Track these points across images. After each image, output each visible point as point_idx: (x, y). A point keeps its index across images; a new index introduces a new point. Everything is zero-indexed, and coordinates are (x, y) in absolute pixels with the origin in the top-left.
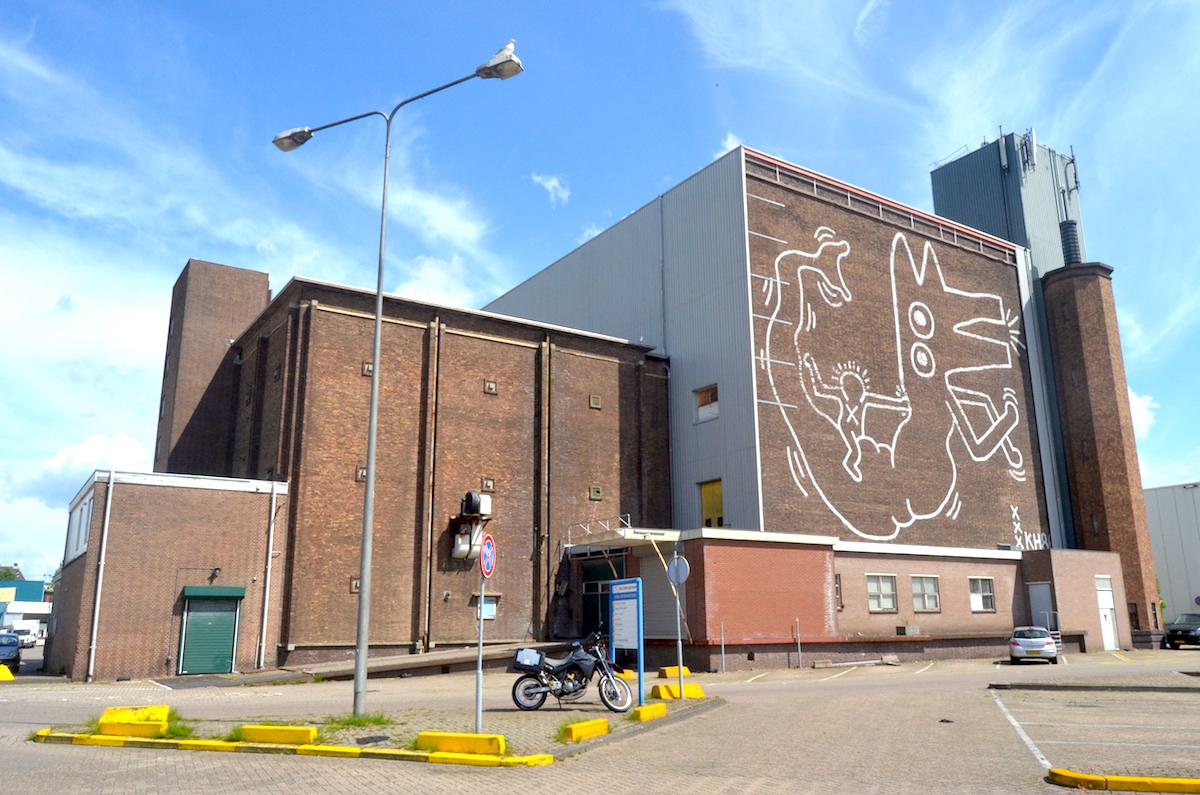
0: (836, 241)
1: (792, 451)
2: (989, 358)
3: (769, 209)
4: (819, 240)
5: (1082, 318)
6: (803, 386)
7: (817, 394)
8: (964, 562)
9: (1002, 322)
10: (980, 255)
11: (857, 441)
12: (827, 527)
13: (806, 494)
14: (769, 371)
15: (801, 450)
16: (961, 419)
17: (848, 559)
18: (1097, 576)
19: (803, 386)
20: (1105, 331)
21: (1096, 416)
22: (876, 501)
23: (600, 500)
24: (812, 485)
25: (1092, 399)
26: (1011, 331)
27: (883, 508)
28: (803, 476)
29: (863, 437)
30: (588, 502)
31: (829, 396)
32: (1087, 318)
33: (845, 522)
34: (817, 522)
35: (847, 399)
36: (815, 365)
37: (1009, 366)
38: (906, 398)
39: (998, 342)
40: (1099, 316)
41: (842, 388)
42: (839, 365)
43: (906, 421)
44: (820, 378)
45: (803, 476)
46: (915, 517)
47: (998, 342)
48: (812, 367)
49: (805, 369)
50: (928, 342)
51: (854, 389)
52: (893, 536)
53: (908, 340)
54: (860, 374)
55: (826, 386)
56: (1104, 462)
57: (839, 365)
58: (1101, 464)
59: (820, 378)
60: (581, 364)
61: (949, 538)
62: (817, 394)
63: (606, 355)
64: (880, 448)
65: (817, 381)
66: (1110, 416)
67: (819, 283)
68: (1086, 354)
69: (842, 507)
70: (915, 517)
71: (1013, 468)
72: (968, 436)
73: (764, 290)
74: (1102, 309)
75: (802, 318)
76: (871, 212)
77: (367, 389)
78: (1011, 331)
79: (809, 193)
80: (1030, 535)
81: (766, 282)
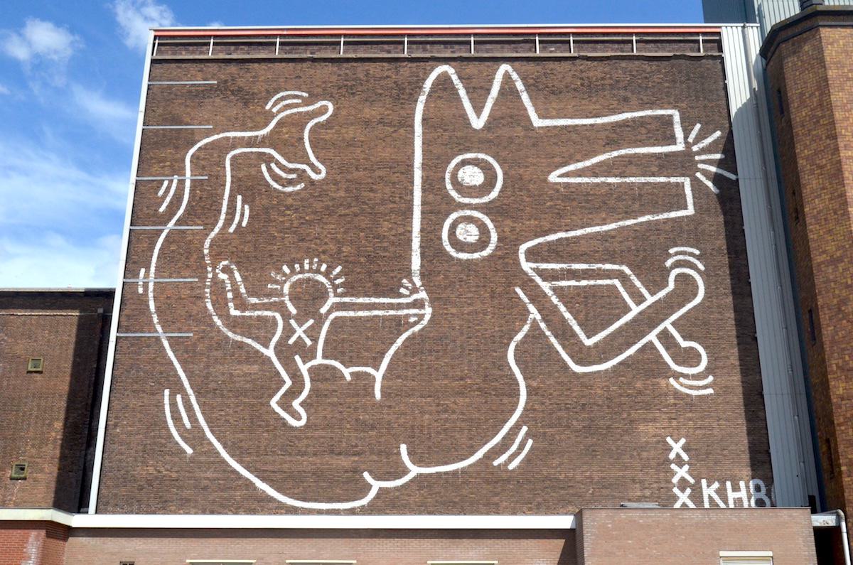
0: (307, 105)
1: (173, 396)
2: (636, 206)
3: (190, 92)
4: (274, 110)
5: (794, 105)
6: (209, 306)
7: (234, 312)
8: (498, 537)
9: (680, 147)
10: (574, 58)
11: (304, 369)
12: (226, 495)
13: (189, 451)
14: (151, 295)
15: (190, 391)
16: (549, 314)
17: (150, 540)
18: (722, 553)
19: (209, 306)
20: (832, 115)
21: (819, 264)
22: (332, 451)
23: (25, 479)
24: (204, 437)
25: (811, 236)
26: (697, 158)
27: (345, 462)
28: (188, 425)
29: (319, 360)
30: (9, 481)
31: (257, 313)
32: (802, 102)
33: (261, 485)
34: (205, 488)
35: (293, 311)
36: (237, 276)
37: (690, 211)
38: (423, 295)
39: (663, 179)
40: (821, 95)
41: (286, 298)
42: (339, 269)
43: (417, 328)
44: (243, 290)
45: (188, 425)
46: (415, 470)
47: (663, 179)
48: (232, 277)
49: (218, 286)
50: (486, 209)
51: (309, 298)
52: (364, 502)
53: (438, 207)
54: (327, 274)
55: (254, 300)
56: (833, 342)
57: (339, 269)
58: (827, 347)
59: (243, 290)
60: (24, 324)
61: (496, 499)
62: (234, 312)
63: (60, 308)
64: (352, 374)
65: (235, 290)
66: (840, 260)
67: (264, 168)
68: (801, 162)
69: (258, 465)
70: (415, 470)
71: (677, 376)
72: (565, 334)
73: (161, 193)
74: (826, 80)
75: (223, 216)
76: (389, 52)
77: (115, 389)
78: (697, 158)
79: (567, 55)
80: (716, 485)
81: (166, 183)
